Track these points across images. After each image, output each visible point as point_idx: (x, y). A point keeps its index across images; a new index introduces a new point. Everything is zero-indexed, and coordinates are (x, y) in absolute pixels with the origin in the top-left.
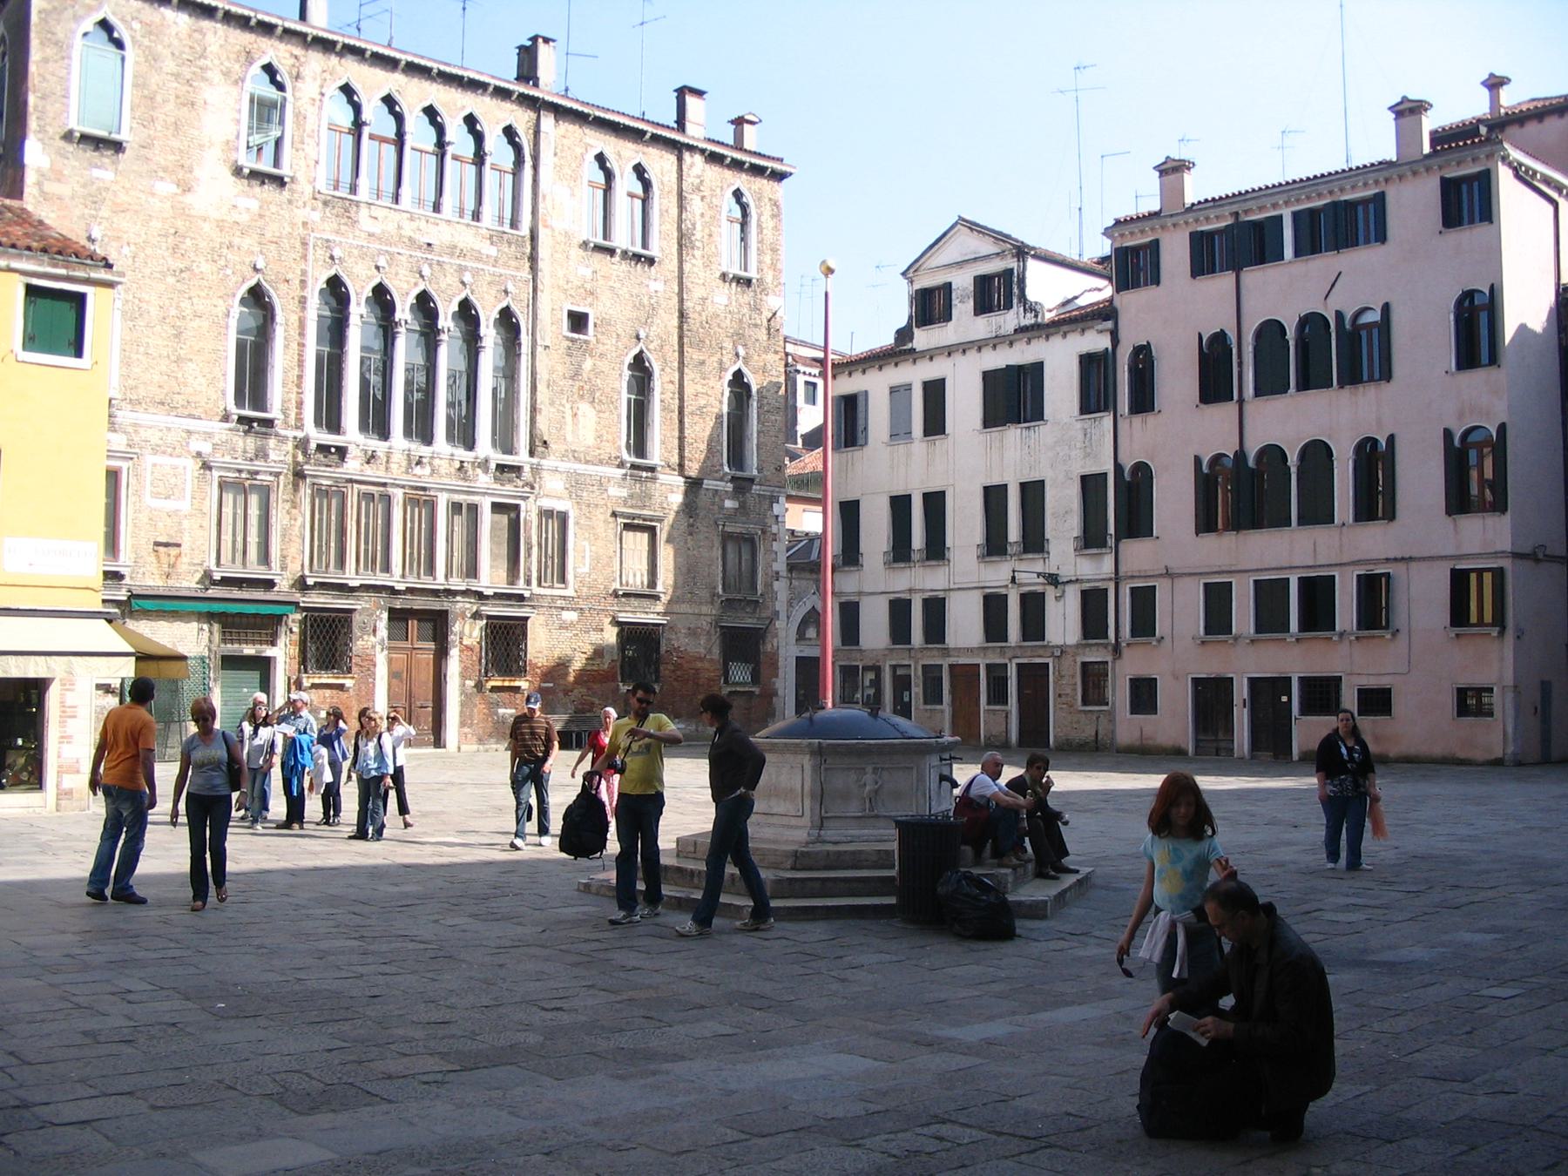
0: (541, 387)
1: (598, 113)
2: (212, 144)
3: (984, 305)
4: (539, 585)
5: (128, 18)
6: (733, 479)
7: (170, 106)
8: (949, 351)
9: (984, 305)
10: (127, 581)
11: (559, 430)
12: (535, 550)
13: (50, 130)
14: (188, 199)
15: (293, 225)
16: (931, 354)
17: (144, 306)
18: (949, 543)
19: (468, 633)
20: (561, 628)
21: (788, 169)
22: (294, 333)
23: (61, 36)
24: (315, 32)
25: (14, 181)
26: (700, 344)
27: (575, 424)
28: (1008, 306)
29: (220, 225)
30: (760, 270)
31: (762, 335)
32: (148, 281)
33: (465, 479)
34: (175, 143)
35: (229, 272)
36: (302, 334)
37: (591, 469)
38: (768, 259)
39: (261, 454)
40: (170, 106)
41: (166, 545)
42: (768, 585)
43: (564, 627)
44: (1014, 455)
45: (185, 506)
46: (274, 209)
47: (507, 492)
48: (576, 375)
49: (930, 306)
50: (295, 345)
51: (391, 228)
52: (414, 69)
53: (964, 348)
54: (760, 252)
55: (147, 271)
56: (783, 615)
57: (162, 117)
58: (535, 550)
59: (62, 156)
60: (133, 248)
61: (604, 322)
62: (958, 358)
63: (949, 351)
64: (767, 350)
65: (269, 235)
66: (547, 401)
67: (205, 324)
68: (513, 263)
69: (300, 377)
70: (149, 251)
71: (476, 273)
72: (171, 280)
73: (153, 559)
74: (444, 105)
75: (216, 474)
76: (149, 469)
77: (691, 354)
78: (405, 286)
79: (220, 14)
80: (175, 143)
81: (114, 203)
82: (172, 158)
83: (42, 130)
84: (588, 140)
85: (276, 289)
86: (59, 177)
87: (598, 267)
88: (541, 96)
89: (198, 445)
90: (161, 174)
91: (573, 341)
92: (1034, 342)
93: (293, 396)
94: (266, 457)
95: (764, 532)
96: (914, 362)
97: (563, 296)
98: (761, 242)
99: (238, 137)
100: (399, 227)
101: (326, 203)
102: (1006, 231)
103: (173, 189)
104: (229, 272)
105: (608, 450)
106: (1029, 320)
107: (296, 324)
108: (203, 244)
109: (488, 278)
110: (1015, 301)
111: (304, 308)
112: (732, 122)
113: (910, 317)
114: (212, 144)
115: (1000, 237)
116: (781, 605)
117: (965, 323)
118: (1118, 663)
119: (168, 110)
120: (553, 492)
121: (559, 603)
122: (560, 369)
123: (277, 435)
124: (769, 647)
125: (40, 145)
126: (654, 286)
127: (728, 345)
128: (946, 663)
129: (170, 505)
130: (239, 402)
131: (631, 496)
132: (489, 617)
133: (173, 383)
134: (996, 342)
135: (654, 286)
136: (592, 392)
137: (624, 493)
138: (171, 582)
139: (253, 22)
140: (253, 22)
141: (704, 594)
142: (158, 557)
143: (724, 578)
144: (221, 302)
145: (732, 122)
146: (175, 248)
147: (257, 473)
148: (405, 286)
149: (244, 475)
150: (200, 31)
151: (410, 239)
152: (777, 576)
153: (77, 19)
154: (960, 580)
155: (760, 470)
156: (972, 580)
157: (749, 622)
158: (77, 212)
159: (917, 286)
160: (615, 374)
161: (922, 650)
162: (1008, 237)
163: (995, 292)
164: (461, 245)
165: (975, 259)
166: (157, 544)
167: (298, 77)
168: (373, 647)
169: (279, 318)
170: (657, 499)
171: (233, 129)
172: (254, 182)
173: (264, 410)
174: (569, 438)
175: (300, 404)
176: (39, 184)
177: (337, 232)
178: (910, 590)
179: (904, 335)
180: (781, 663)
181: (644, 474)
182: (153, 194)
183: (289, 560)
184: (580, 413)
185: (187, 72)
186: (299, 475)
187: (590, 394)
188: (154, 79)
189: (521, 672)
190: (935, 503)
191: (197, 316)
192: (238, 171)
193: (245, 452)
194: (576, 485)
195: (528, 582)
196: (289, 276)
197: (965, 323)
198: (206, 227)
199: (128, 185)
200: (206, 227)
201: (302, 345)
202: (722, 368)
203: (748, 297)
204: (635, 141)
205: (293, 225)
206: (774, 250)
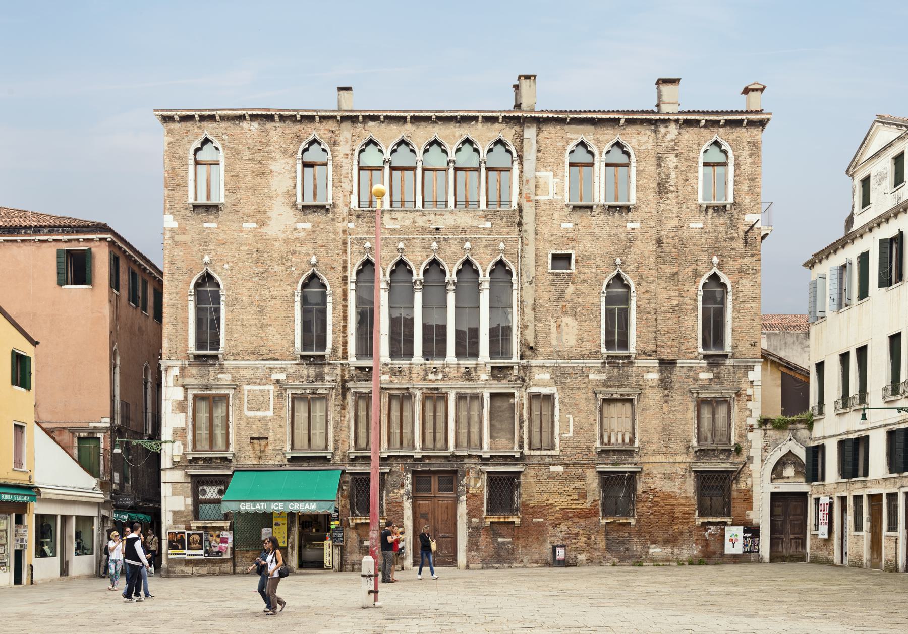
1: (461, 114)
2: (278, 195)
5: (220, 134)
6: (706, 357)
7: (249, 178)
10: (234, 462)
12: (526, 424)
14: (264, 230)
15: (335, 233)
17: (239, 297)
19: (476, 483)
20: (549, 478)
22: (339, 299)
23: (181, 153)
29: (286, 242)
31: (739, 245)
32: (241, 282)
33: (469, 380)
34: (253, 199)
35: (293, 269)
36: (345, 300)
37: (573, 363)
38: (745, 187)
39: (320, 377)
40: (249, 178)
41: (258, 439)
43: (553, 476)
45: (270, 414)
46: (322, 226)
48: (560, 297)
50: (340, 307)
51: (407, 223)
52: (416, 120)
55: (240, 276)
56: (757, 460)
57: (243, 186)
58: (526, 424)
59: (185, 219)
60: (230, 264)
61: (584, 259)
64: (743, 256)
65: (319, 242)
67: (279, 302)
68: (505, 230)
69: (345, 327)
70: (240, 264)
71: (474, 241)
72: (255, 279)
73: (250, 448)
74: (445, 138)
75: (289, 392)
76: (246, 393)
78: (420, 258)
79: (277, 118)
80: (253, 199)
81: (218, 240)
84: (569, 135)
85: (326, 275)
86: (183, 231)
87: (578, 221)
89: (275, 376)
91: (557, 275)
93: (340, 339)
94: (323, 378)
95: (738, 394)
99: (295, 187)
100: (414, 222)
101: (358, 216)
103: (254, 225)
104: (293, 269)
105: (589, 347)
107: (341, 294)
108: (275, 255)
109: (485, 243)
111: (346, 283)
114: (278, 195)
118: (46, 493)
119: (248, 180)
120: (542, 381)
121: (547, 460)
123: (329, 364)
124: (742, 486)
125: (171, 217)
126: (630, 225)
127: (704, 257)
129: (260, 414)
130: (705, 345)
131: (610, 379)
132: (488, 473)
133: (259, 340)
135: (630, 225)
136: (574, 309)
137: (604, 377)
138: (261, 462)
139: (298, 118)
140: (298, 118)
141: (680, 447)
142: (253, 447)
143: (698, 434)
144: (289, 288)
146: (257, 260)
147: (317, 389)
149: (308, 391)
150: (266, 131)
151: (422, 227)
152: (751, 429)
153: (190, 142)
157: (719, 465)
158: (196, 249)
160: (595, 293)
164: (462, 225)
166: (252, 439)
167: (335, 143)
168: (402, 497)
169: (329, 291)
170: (633, 379)
171: (291, 183)
172: (307, 212)
174: (554, 342)
175: (345, 344)
177: (367, 233)
180: (755, 498)
181: (621, 362)
183: (340, 443)
185: (258, 157)
186: (345, 390)
188: (238, 165)
189: (513, 511)
191: (273, 298)
192: (294, 205)
193: (308, 377)
194: (559, 375)
195: (521, 446)
196: (335, 265)
200: (277, 244)
201: (345, 307)
202: (697, 274)
203: (724, 219)
204: (695, 129)
205: (335, 233)
206: (752, 179)
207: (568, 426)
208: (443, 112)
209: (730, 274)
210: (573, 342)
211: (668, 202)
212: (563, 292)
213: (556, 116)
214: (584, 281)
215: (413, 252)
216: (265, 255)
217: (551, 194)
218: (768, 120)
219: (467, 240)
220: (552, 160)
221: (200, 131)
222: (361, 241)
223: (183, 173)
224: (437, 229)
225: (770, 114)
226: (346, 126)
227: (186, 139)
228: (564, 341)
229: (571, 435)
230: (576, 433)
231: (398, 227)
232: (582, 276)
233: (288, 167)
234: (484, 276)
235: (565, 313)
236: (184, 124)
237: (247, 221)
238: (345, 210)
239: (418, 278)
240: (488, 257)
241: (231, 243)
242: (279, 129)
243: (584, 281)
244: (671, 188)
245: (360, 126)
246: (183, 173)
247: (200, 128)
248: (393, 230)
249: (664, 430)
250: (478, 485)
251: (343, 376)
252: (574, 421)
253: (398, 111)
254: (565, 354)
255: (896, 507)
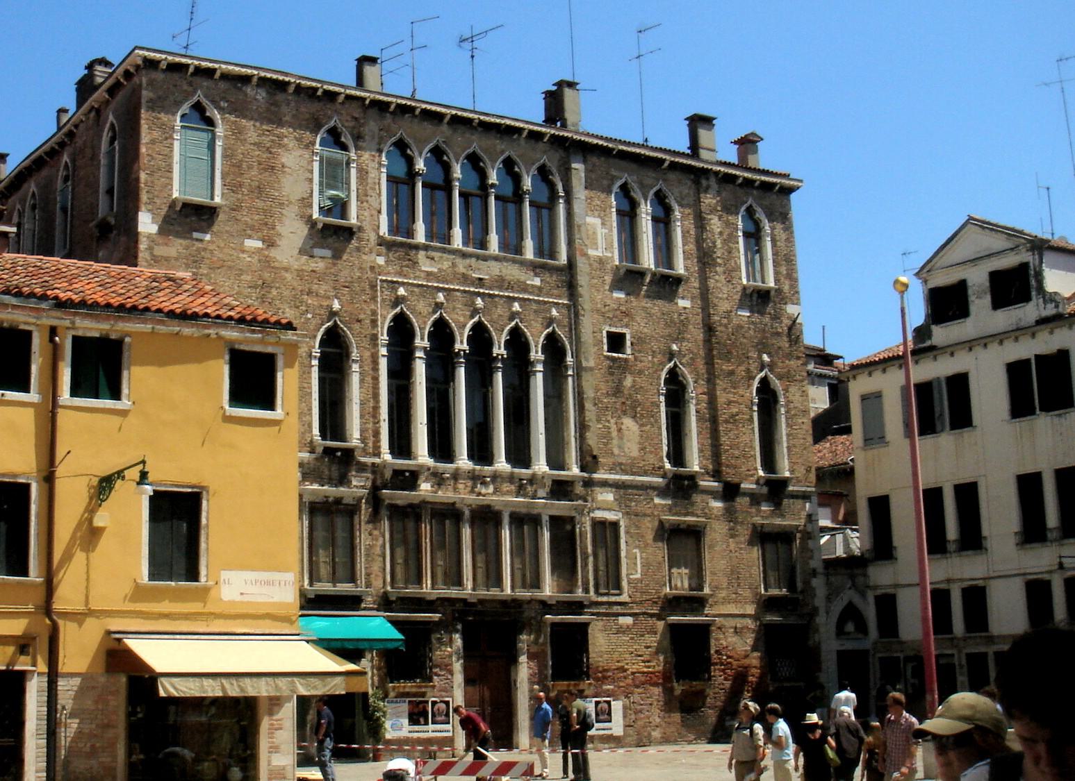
0: (588, 405)
3: (999, 302)
4: (597, 592)
5: (217, 98)
7: (254, 172)
8: (969, 345)
9: (999, 302)
11: (606, 444)
13: (158, 201)
14: (273, 253)
16: (950, 349)
18: (985, 532)
21: (796, 183)
24: (372, 96)
25: (128, 249)
26: (727, 356)
27: (621, 438)
28: (1027, 299)
30: (777, 281)
31: (784, 343)
35: (309, 316)
38: (783, 270)
40: (254, 172)
42: (807, 583)
43: (621, 630)
44: (944, 460)
47: (561, 507)
49: (947, 303)
51: (446, 265)
53: (984, 341)
54: (776, 264)
56: (822, 612)
58: (591, 559)
62: (978, 350)
63: (969, 345)
66: (594, 418)
77: (723, 366)
80: (260, 204)
82: (257, 217)
83: (151, 201)
84: (614, 172)
88: (570, 135)
90: (249, 232)
91: (613, 360)
92: (1057, 331)
93: (370, 426)
96: (935, 358)
97: (601, 319)
98: (775, 254)
100: (454, 265)
102: (1018, 227)
103: (259, 244)
104: (309, 316)
105: (651, 459)
106: (1050, 311)
107: (369, 360)
110: (1034, 293)
112: (735, 143)
113: (927, 316)
115: (1012, 233)
116: (820, 601)
117: (983, 316)
119: (253, 175)
120: (605, 504)
122: (604, 388)
128: (991, 650)
134: (1018, 332)
136: (634, 408)
139: (319, 93)
141: (747, 593)
145: (735, 143)
148: (462, 319)
150: (275, 104)
152: (814, 573)
154: (1001, 568)
155: (792, 471)
156: (1010, 567)
159: (932, 285)
161: (965, 639)
162: (1021, 232)
163: (1013, 286)
165: (989, 256)
168: (450, 656)
173: (344, 440)
174: (616, 451)
176: (150, 249)
178: (949, 581)
179: (922, 333)
182: (243, 252)
184: (623, 427)
187: (633, 408)
190: (968, 494)
195: (586, 590)
196: (362, 316)
197: (983, 316)
198: (288, 276)
199: (222, 245)
200: (288, 276)
207: (635, 564)
208: (487, 115)
209: (780, 378)
210: (635, 453)
211: (717, 277)
212: (620, 381)
213: (605, 144)
214: (640, 372)
215: (454, 308)
216: (274, 292)
217: (600, 250)
218: (798, 188)
219: (514, 299)
220: (599, 203)
221: (190, 89)
222: (394, 285)
223: (166, 151)
224: (481, 279)
225: (801, 181)
226: (373, 112)
227: (172, 98)
228: (626, 450)
229: (638, 576)
230: (644, 574)
231: (436, 270)
232: (640, 365)
233: (304, 163)
234: (537, 352)
235: (624, 413)
236: (169, 75)
237: (250, 237)
238: (373, 238)
239: (499, 352)
240: (539, 326)
241: (230, 268)
242: (293, 104)
243: (640, 372)
244: (718, 260)
245: (388, 119)
246: (166, 151)
247: (190, 84)
248: (429, 274)
249: (732, 572)
250: (541, 640)
251: (374, 482)
252: (641, 558)
253: (237, 65)
254: (628, 468)
255: (567, 765)
